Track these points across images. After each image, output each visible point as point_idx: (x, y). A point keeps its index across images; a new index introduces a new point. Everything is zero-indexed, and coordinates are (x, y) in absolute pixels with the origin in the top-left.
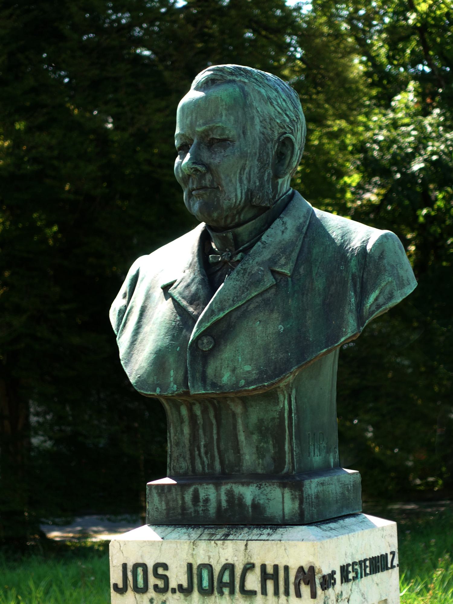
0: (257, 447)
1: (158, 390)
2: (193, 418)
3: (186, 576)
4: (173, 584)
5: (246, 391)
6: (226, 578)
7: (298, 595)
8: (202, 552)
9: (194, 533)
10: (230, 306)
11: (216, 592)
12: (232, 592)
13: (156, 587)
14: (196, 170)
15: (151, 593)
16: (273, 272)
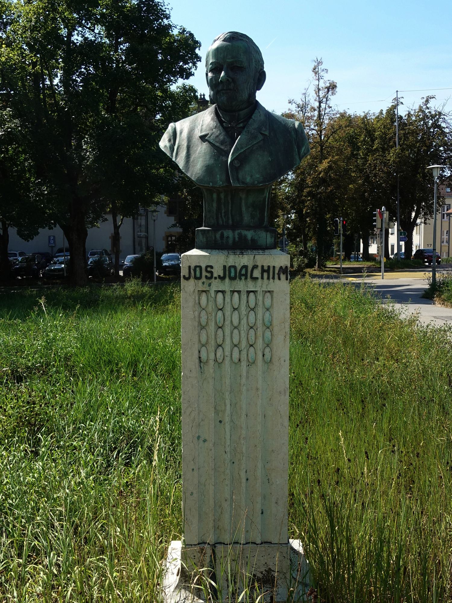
0: (251, 214)
1: (211, 184)
2: (219, 199)
3: (223, 271)
4: (215, 275)
5: (258, 186)
6: (243, 272)
7: (279, 279)
8: (231, 260)
9: (226, 252)
10: (245, 147)
11: (238, 278)
12: (246, 278)
13: (206, 277)
14: (228, 80)
15: (204, 279)
16: (261, 134)
